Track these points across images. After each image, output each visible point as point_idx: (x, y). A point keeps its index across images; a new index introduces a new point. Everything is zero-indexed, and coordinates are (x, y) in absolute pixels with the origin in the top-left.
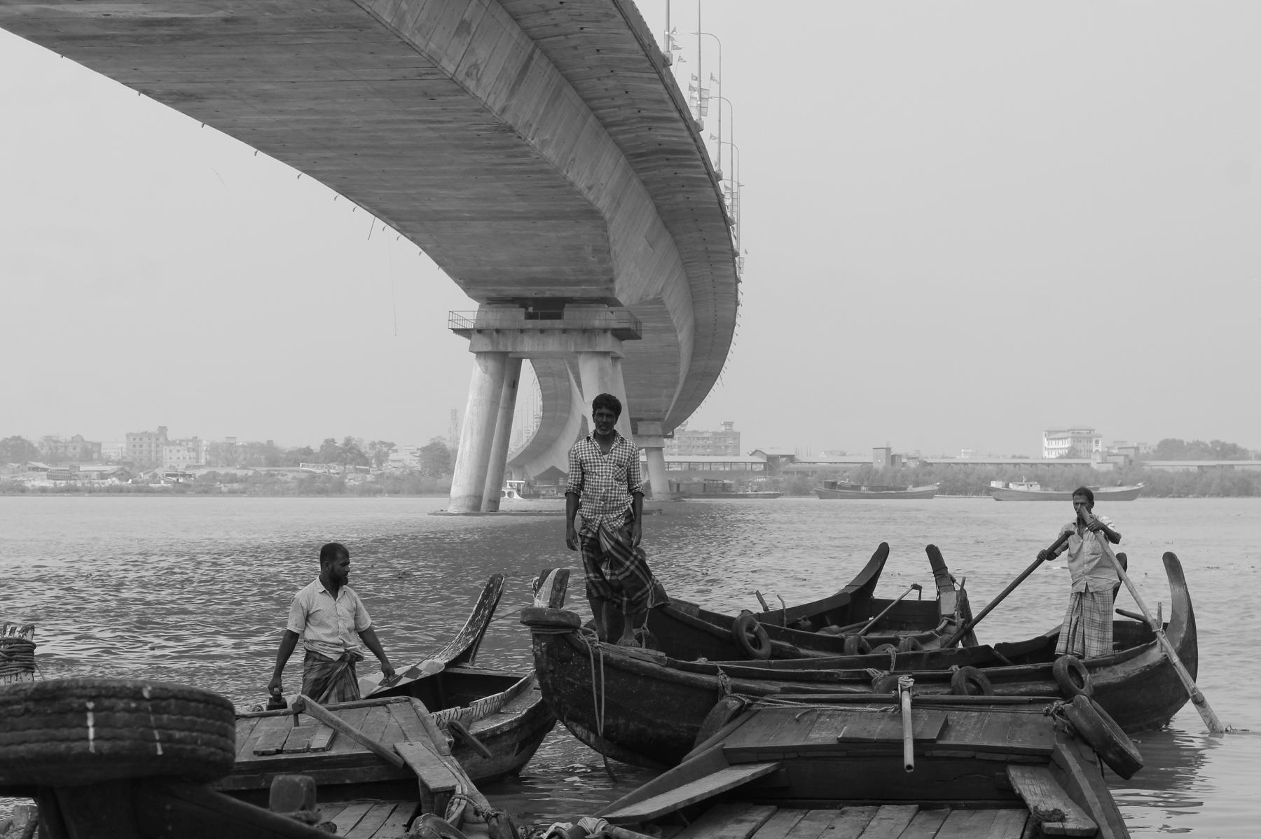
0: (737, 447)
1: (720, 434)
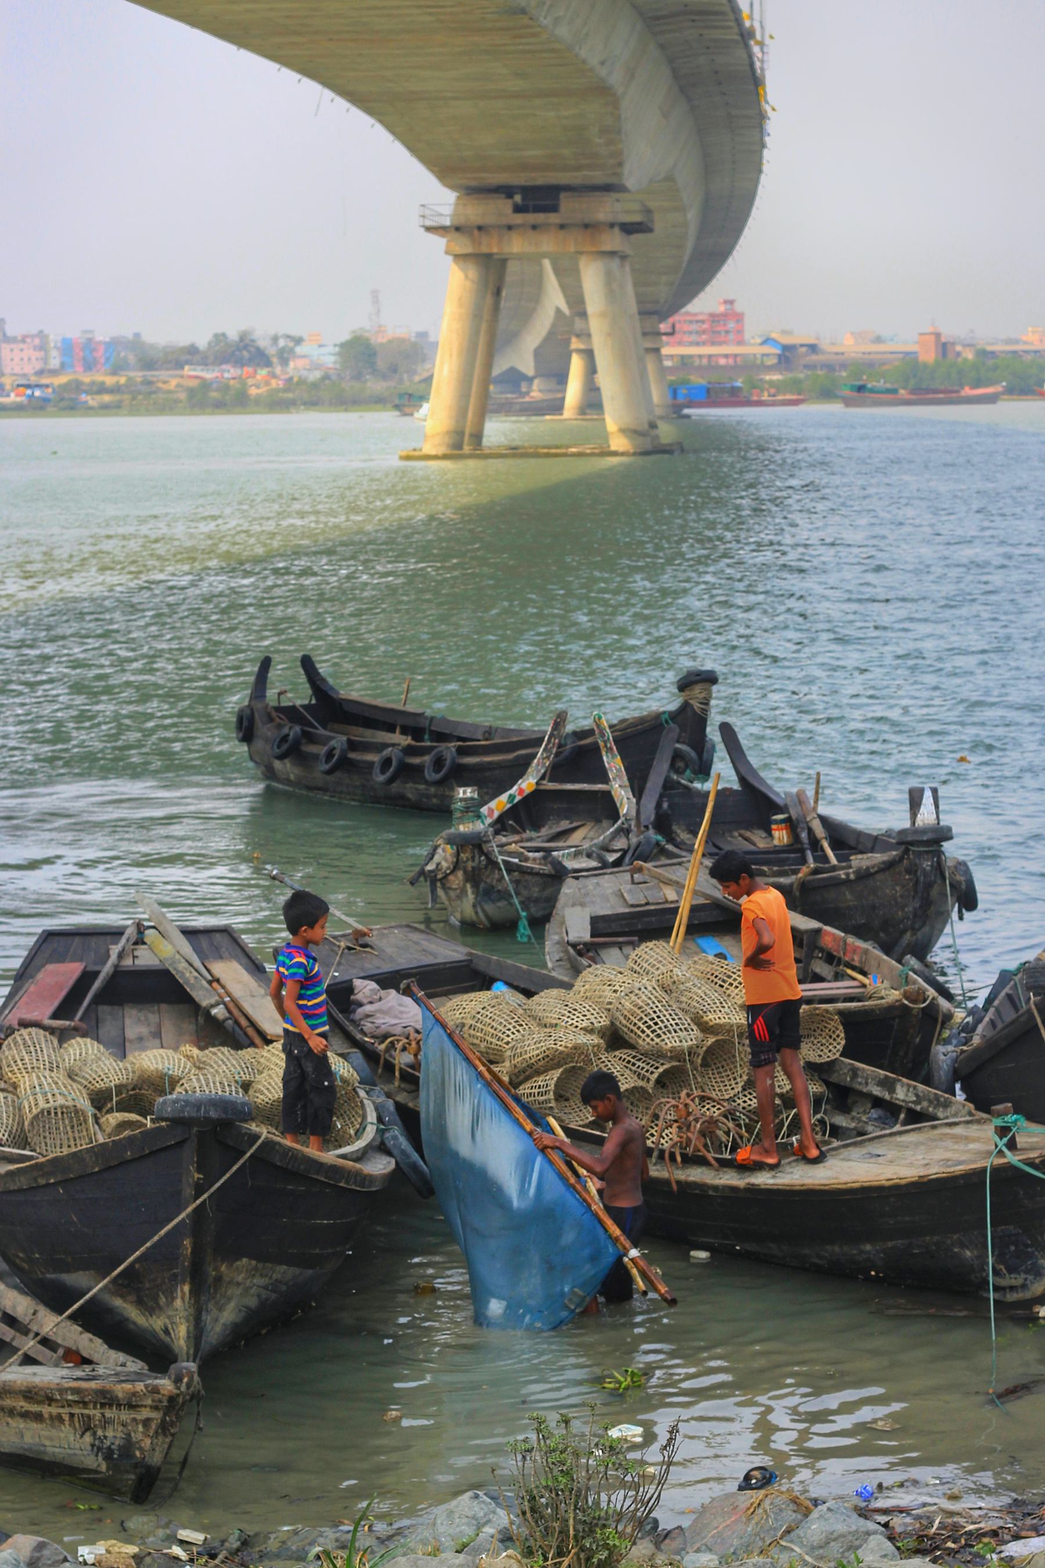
0: (740, 331)
1: (718, 315)
